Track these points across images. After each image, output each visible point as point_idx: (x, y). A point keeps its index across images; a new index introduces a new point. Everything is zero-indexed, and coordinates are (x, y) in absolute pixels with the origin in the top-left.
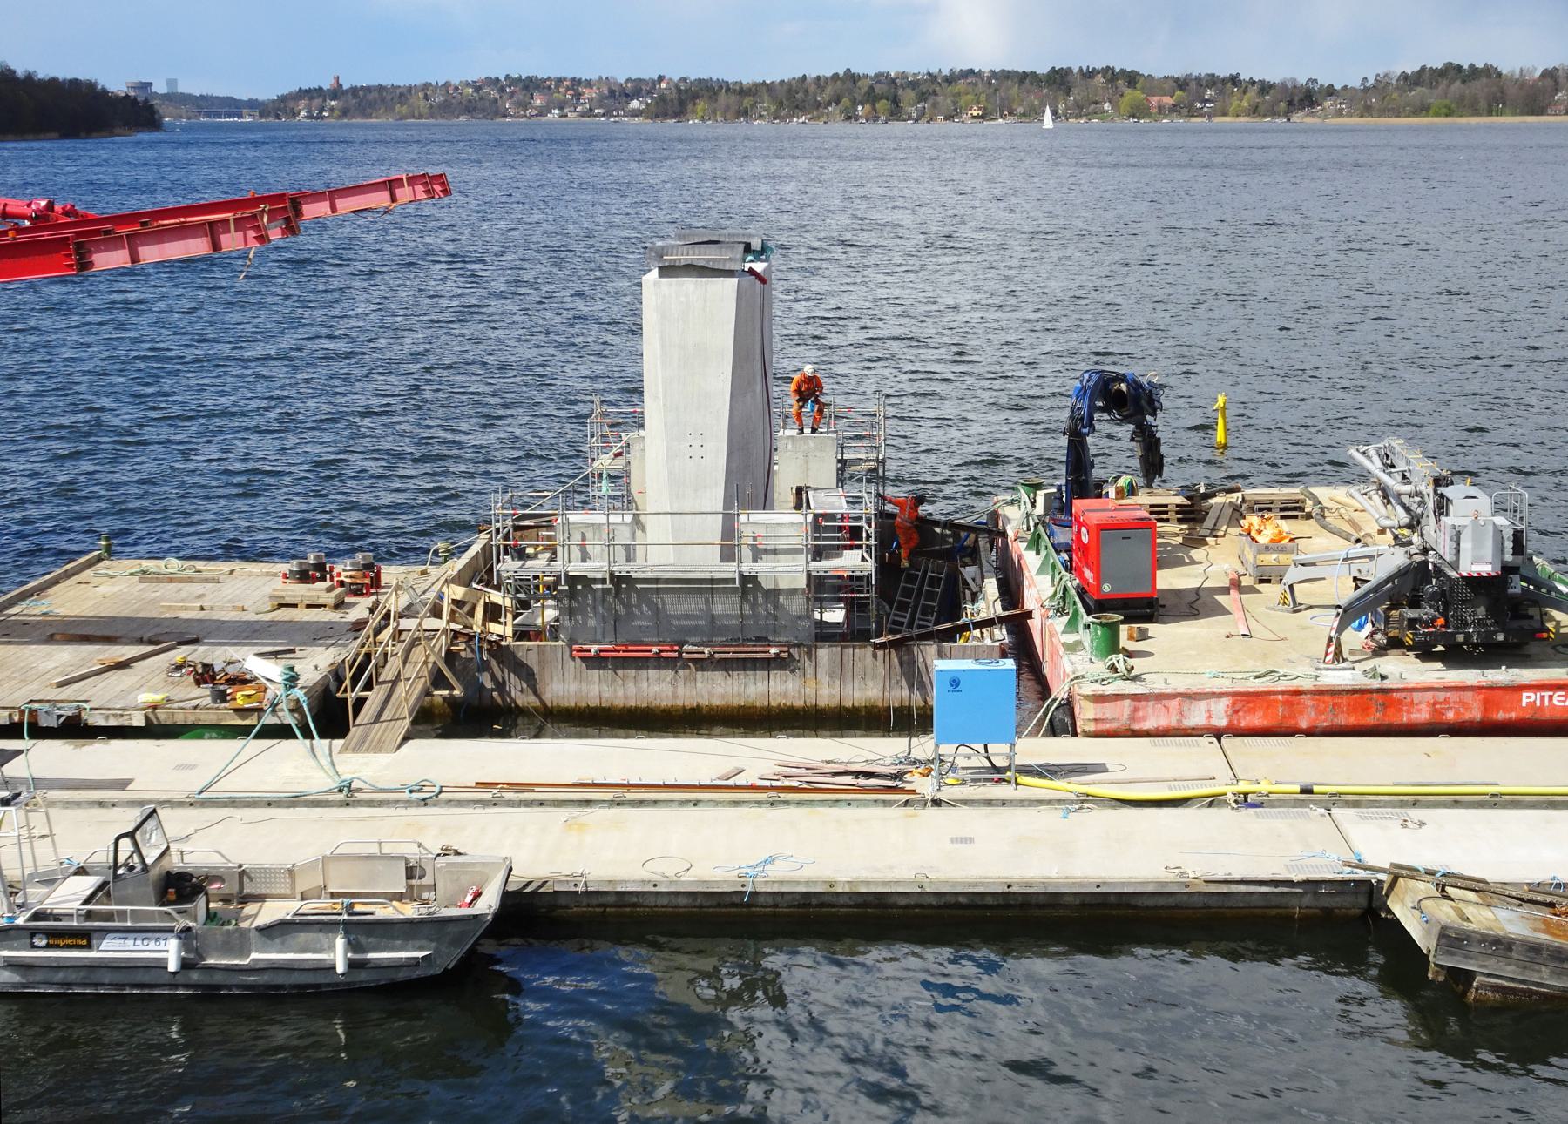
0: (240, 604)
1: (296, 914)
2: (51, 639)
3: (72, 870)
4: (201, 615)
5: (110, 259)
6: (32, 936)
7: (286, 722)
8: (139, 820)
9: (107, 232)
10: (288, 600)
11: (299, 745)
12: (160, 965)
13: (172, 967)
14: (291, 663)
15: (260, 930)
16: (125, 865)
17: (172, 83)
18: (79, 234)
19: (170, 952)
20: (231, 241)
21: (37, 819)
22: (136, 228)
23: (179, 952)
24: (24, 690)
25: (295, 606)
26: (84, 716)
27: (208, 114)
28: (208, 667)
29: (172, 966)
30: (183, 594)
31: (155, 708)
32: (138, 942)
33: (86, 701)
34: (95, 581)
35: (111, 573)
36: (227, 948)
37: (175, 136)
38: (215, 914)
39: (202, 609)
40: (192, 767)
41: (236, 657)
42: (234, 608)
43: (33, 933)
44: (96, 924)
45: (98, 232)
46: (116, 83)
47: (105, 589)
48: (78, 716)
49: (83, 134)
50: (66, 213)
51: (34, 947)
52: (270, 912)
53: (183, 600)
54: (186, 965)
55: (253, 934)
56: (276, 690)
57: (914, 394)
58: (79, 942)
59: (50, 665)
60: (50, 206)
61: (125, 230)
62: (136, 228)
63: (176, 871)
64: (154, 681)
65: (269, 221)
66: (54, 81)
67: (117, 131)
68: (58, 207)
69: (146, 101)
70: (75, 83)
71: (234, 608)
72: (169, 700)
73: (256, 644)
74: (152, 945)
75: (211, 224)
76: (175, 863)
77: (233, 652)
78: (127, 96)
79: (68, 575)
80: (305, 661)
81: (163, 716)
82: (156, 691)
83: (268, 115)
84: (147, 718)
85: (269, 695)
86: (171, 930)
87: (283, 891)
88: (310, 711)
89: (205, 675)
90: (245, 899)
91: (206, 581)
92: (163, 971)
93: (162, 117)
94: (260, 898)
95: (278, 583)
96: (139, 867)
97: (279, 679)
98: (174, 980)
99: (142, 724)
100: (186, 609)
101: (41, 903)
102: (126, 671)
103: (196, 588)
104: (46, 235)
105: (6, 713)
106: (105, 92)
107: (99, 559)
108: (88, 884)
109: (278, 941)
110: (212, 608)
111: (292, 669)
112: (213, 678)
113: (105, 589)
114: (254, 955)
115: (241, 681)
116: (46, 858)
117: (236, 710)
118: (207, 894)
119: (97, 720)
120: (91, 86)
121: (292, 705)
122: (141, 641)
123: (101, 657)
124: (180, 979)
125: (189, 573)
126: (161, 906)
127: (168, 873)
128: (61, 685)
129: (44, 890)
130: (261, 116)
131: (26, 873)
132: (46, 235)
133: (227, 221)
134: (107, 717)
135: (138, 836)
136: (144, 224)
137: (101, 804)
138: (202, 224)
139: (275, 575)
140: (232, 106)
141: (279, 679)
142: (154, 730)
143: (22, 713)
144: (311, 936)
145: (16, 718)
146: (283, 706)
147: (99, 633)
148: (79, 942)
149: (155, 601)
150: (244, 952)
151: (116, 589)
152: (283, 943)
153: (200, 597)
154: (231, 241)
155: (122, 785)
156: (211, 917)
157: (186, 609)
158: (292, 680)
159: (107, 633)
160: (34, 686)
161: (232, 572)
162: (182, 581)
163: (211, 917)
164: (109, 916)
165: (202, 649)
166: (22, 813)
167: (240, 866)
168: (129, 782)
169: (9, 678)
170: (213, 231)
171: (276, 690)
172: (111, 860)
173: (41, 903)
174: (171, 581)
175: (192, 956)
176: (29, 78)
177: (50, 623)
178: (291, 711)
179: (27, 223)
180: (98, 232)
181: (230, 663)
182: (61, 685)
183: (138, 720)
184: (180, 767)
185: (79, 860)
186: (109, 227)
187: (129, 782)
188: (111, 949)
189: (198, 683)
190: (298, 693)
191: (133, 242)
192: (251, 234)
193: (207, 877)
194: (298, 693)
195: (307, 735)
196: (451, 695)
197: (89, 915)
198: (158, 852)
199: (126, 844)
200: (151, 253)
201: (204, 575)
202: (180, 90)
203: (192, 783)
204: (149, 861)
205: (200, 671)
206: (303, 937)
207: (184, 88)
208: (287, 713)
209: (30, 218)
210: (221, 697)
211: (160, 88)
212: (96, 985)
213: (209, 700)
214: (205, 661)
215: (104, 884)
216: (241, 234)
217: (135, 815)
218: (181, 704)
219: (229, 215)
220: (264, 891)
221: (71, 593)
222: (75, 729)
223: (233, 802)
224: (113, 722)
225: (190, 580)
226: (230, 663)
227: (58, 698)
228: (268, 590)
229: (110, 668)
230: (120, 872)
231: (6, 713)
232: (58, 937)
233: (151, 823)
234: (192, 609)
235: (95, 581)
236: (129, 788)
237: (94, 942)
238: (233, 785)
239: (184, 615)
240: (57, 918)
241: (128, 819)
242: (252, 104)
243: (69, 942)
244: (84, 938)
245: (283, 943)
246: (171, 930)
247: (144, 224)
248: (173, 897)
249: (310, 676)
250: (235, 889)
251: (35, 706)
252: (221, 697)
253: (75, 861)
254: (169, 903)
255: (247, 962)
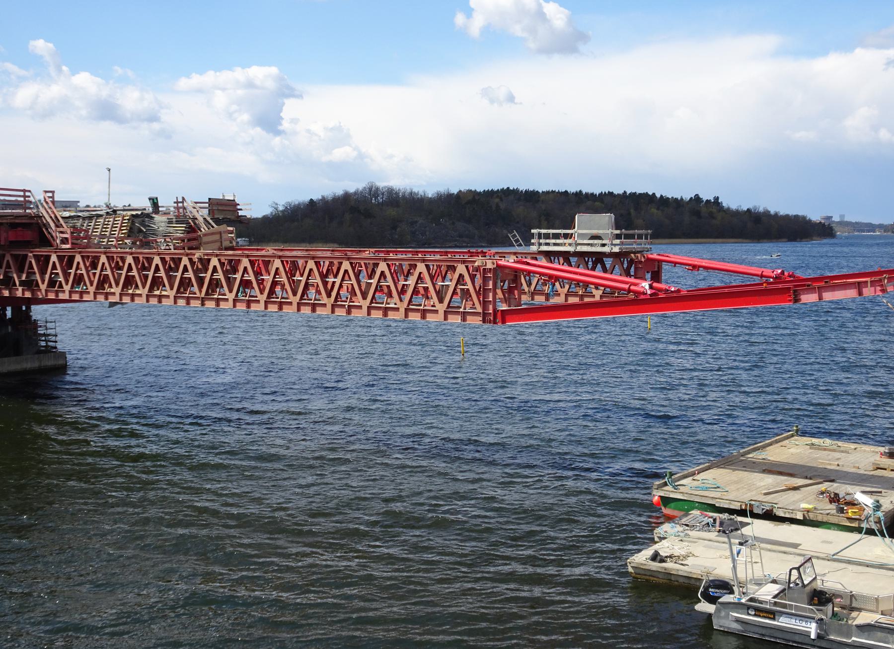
0: (857, 465)
1: (876, 622)
2: (764, 471)
3: (770, 580)
4: (838, 468)
5: (809, 298)
6: (748, 609)
7: (873, 527)
8: (803, 562)
9: (808, 285)
10: (882, 466)
11: (878, 539)
12: (807, 635)
13: (813, 636)
14: (879, 498)
15: (858, 626)
16: (795, 582)
17: (842, 216)
18: (796, 286)
19: (812, 629)
20: (868, 292)
21: (755, 553)
22: (823, 284)
23: (816, 630)
24: (749, 494)
25: (885, 469)
26: (775, 511)
27: (858, 231)
28: (836, 495)
29: (813, 636)
30: (830, 457)
31: (808, 511)
32: (797, 621)
33: (776, 504)
34: (788, 446)
35: (797, 443)
36: (840, 633)
37: (840, 241)
38: (837, 614)
39: (838, 465)
40: (831, 543)
41: (851, 492)
42: (854, 467)
43: (749, 607)
44: (778, 609)
45: (804, 285)
46: (815, 216)
47: (793, 450)
48: (772, 510)
49: (799, 240)
50: (790, 276)
51: (749, 614)
52: (863, 618)
53: (829, 460)
54: (819, 637)
55: (854, 628)
56: (869, 511)
57: (361, 326)
58: (770, 616)
59: (762, 484)
60: (783, 273)
61: (816, 285)
62: (823, 284)
63: (819, 589)
64: (810, 498)
65: (888, 282)
66: (787, 216)
67: (814, 238)
68: (786, 273)
69: (829, 225)
70: (797, 217)
71: (854, 467)
72: (815, 509)
73: (863, 486)
74: (804, 624)
75: (859, 283)
76: (819, 585)
77: (849, 489)
78: (820, 222)
79: (777, 442)
80: (886, 498)
81: (812, 516)
82: (810, 503)
83: (888, 231)
84: (804, 516)
85: (865, 513)
86: (813, 618)
87: (872, 608)
88: (885, 524)
89: (835, 499)
90: (853, 609)
91: (842, 452)
92: (807, 638)
93: (836, 232)
94: (859, 610)
95: (878, 458)
96: (800, 585)
97: (871, 506)
98: (812, 643)
99: (802, 518)
100: (830, 464)
101: (754, 594)
102: (797, 491)
103: (837, 455)
104: (780, 286)
105: (739, 504)
106: (810, 221)
107: (792, 436)
108: (775, 589)
109: (866, 633)
110: (843, 466)
111: (878, 502)
112: (838, 501)
113: (793, 450)
114: (854, 639)
115: (852, 504)
116: (758, 574)
117: (848, 518)
118: (833, 603)
119: (781, 513)
120: (804, 218)
121: (876, 520)
122: (806, 478)
123: (786, 483)
124: (815, 643)
125: (835, 447)
126: (810, 605)
127: (815, 590)
128: (766, 494)
129: (757, 587)
130: (885, 231)
131: (748, 579)
132: (780, 286)
133: (866, 282)
134: (785, 513)
135: (801, 569)
136: (826, 282)
137: (785, 553)
138: (854, 283)
139: (877, 452)
140: (871, 227)
141: (871, 506)
142: (805, 522)
143: (746, 505)
144: (883, 635)
145: (743, 507)
146: (871, 519)
147: (786, 471)
148: (770, 616)
149: (816, 459)
150: (849, 636)
151: (798, 451)
152: (869, 635)
153: (838, 459)
154: (868, 292)
155: (796, 546)
156: (834, 614)
157: (830, 464)
158: (878, 507)
159: (791, 472)
160: (754, 493)
161: (855, 449)
162: (830, 450)
163: (834, 614)
164: (784, 606)
165: (835, 485)
166: (748, 550)
167: (851, 592)
168: (800, 545)
169: (743, 488)
170: (859, 287)
171: (869, 511)
172: (787, 578)
173: (754, 594)
174: (825, 450)
175: (823, 633)
176: (776, 214)
177: (765, 464)
178: (875, 522)
179: (771, 280)
180: (804, 285)
181: (848, 494)
182: (766, 494)
183: (800, 516)
184: (824, 542)
185: (774, 576)
186: (810, 283)
187: (800, 545)
188: (783, 622)
189: (831, 502)
190: (880, 514)
191: (820, 290)
192: (879, 288)
193: (834, 595)
194: (880, 514)
195: (883, 535)
196: (643, 645)
197: (775, 604)
198: (811, 579)
199: (795, 572)
200: (828, 296)
201: (842, 449)
202: (846, 220)
203: (831, 550)
204: (806, 582)
205: (832, 496)
206: (879, 634)
207: (848, 219)
208: (873, 523)
209: (773, 278)
210: (841, 511)
211: (836, 219)
212: (776, 638)
213: (835, 511)
214: (836, 492)
215: (784, 590)
216: (873, 288)
217: (801, 560)
218: (821, 512)
219: (868, 279)
220: (862, 607)
221: (777, 451)
222: (769, 516)
223: (849, 562)
224: (787, 516)
225: (834, 451)
226: (848, 494)
227: (764, 500)
228: (872, 460)
229: (790, 489)
230: (791, 585)
231: (739, 504)
232: (759, 612)
233: (808, 564)
234: (833, 465)
235: (788, 446)
236: (799, 548)
237: (777, 617)
238: (848, 554)
239: (829, 467)
240: (761, 602)
241: (797, 561)
242: (881, 226)
243: (765, 615)
244: (772, 614)
245: (869, 635)
246: (813, 618)
247: (826, 282)
248: (816, 602)
249: (888, 506)
250: (848, 603)
251: (753, 503)
252: (841, 511)
253: (772, 576)
254: (814, 605)
255: (850, 641)
